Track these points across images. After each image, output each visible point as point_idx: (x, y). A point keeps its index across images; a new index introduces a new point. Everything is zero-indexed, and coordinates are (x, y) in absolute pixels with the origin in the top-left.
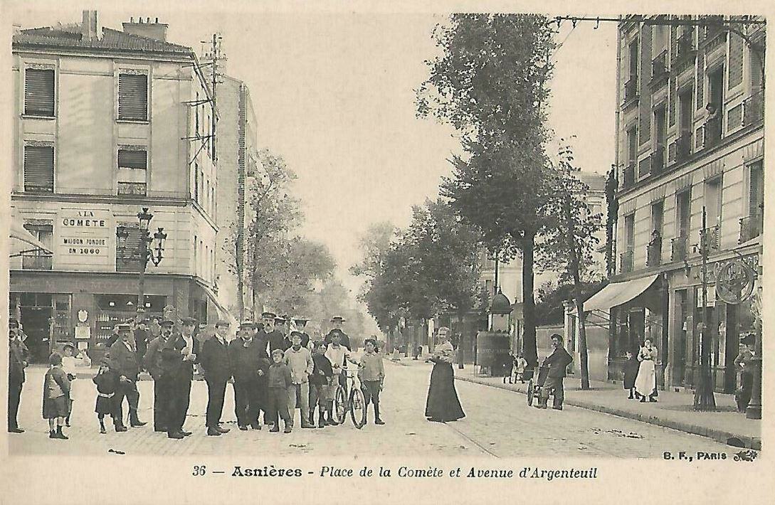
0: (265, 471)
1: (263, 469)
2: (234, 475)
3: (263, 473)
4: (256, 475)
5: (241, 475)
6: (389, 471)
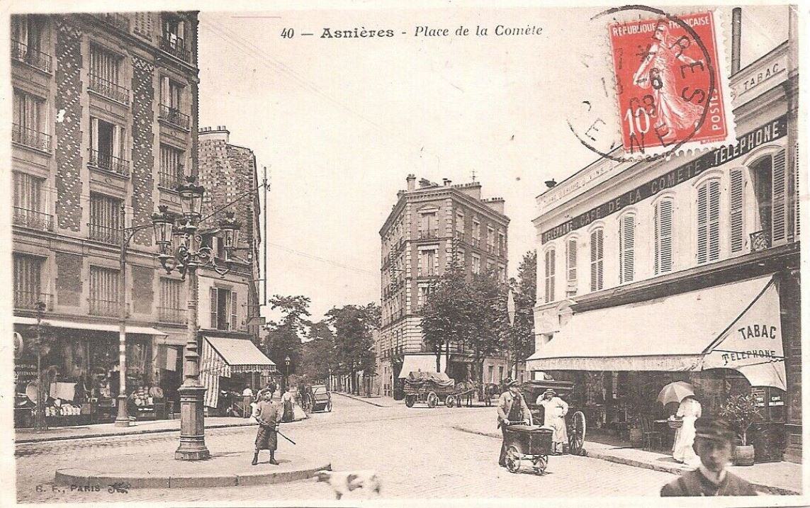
0: (356, 32)
1: (353, 30)
2: (323, 37)
3: (353, 34)
4: (345, 36)
5: (331, 37)
6: (486, 30)
